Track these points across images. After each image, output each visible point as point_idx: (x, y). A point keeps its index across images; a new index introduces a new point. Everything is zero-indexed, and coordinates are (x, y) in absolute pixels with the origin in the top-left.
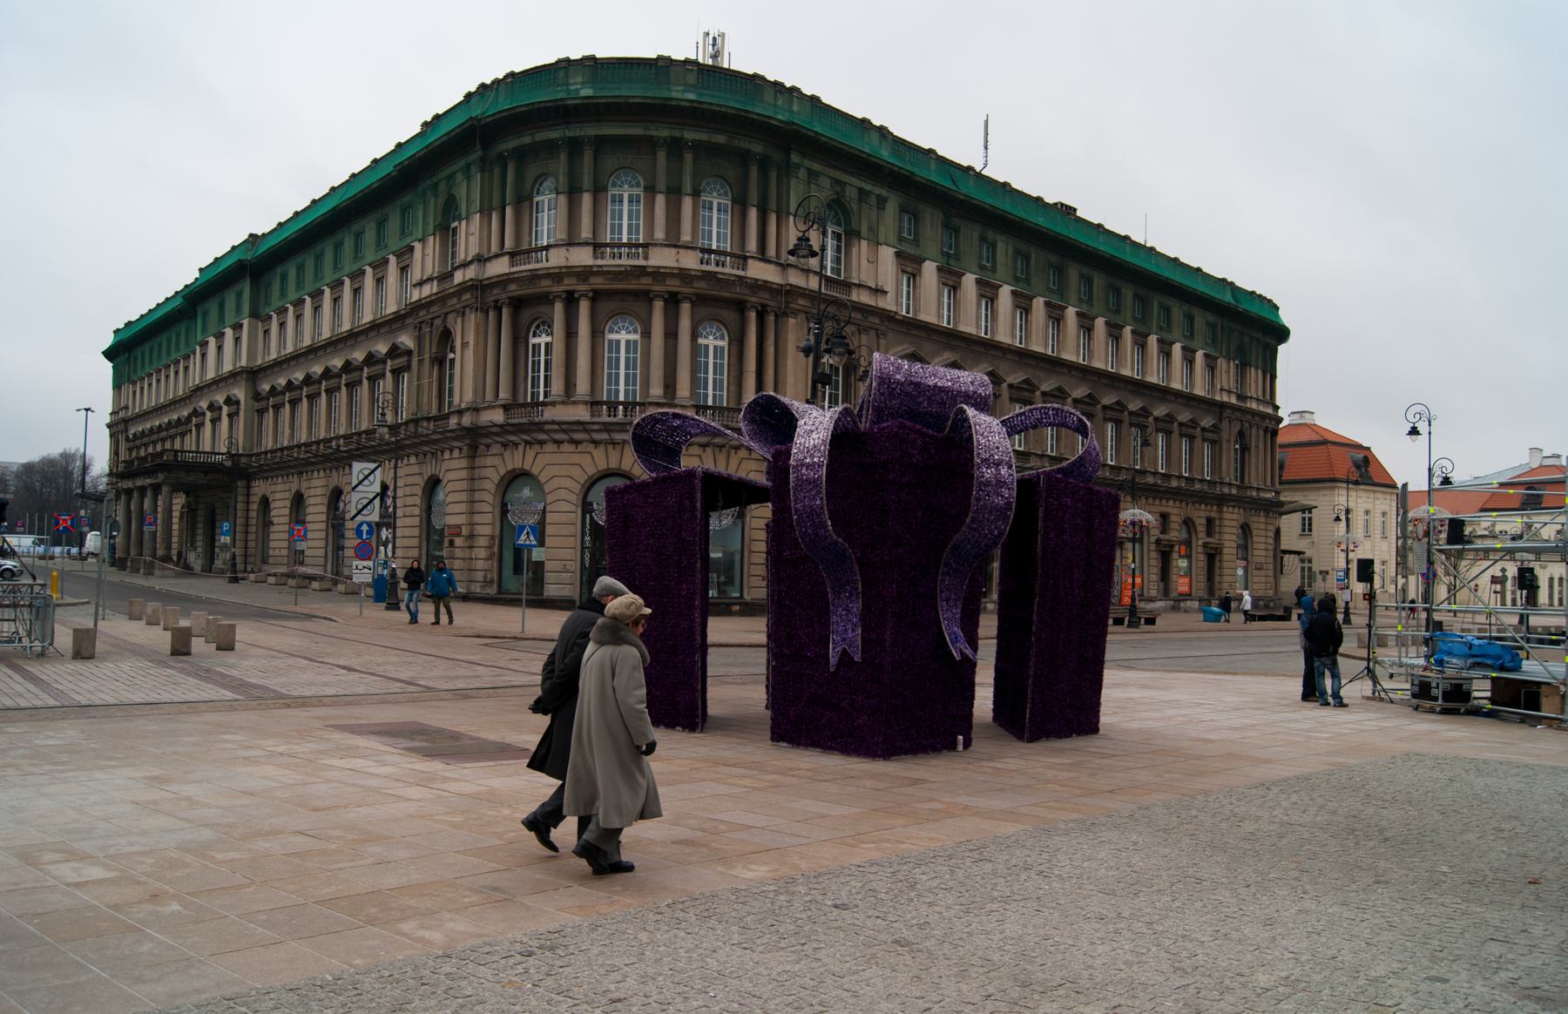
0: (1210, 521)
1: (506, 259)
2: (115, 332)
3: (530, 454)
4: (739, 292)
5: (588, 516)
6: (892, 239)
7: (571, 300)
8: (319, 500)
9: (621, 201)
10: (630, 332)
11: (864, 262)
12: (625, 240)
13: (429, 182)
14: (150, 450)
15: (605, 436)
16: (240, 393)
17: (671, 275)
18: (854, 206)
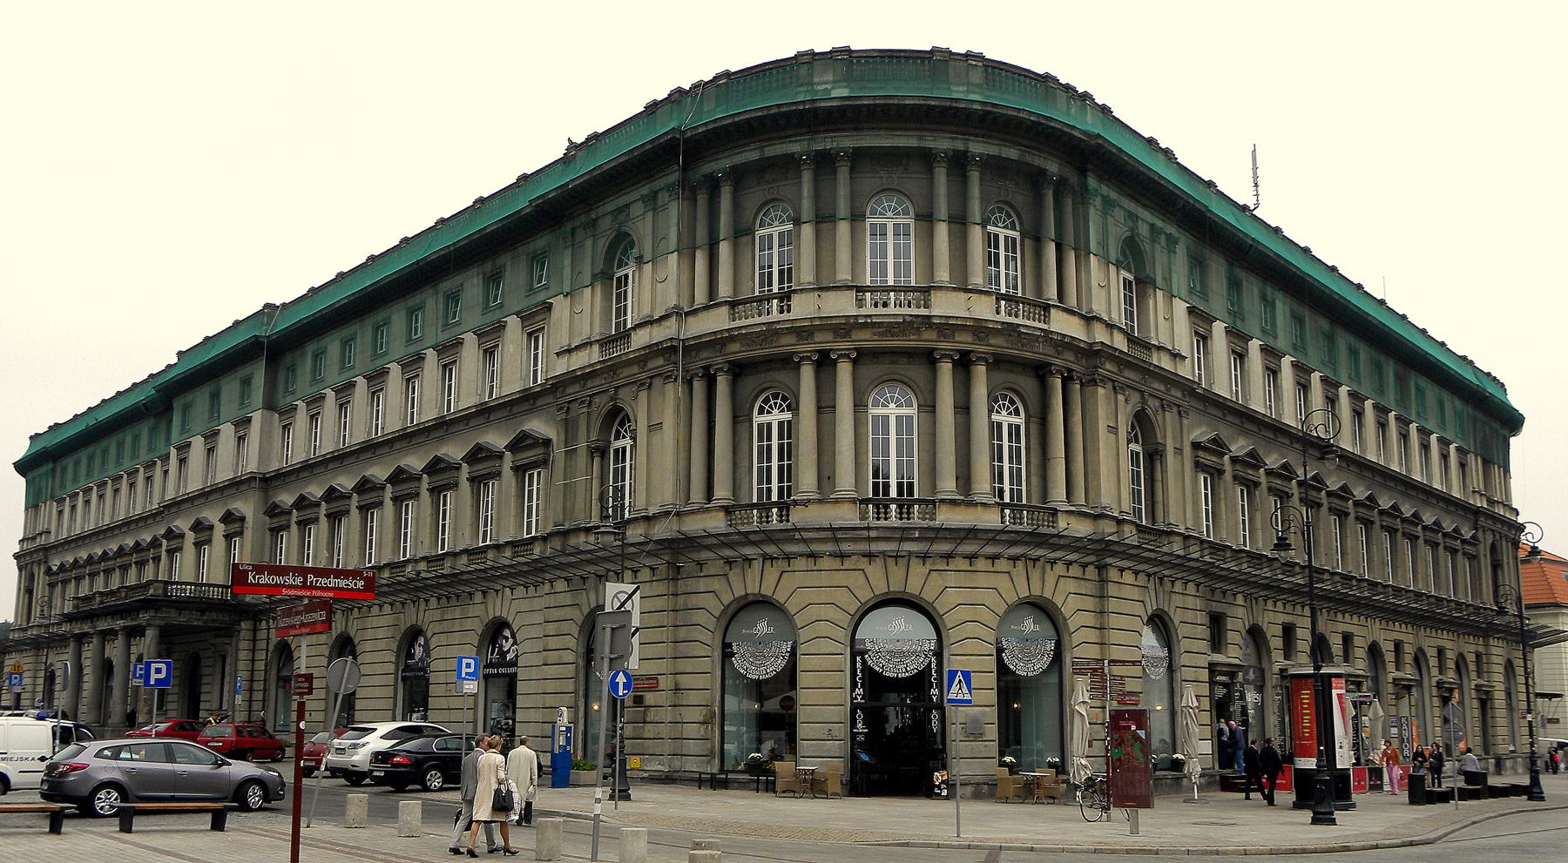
0: (1478, 656)
1: (724, 310)
2: (31, 438)
3: (772, 573)
4: (1040, 352)
5: (858, 659)
6: (1184, 294)
7: (825, 363)
8: (381, 645)
10: (1010, 414)
11: (1161, 319)
12: (891, 282)
13: (583, 218)
14: (99, 585)
15: (829, 547)
16: (247, 507)
17: (963, 328)
18: (1148, 247)
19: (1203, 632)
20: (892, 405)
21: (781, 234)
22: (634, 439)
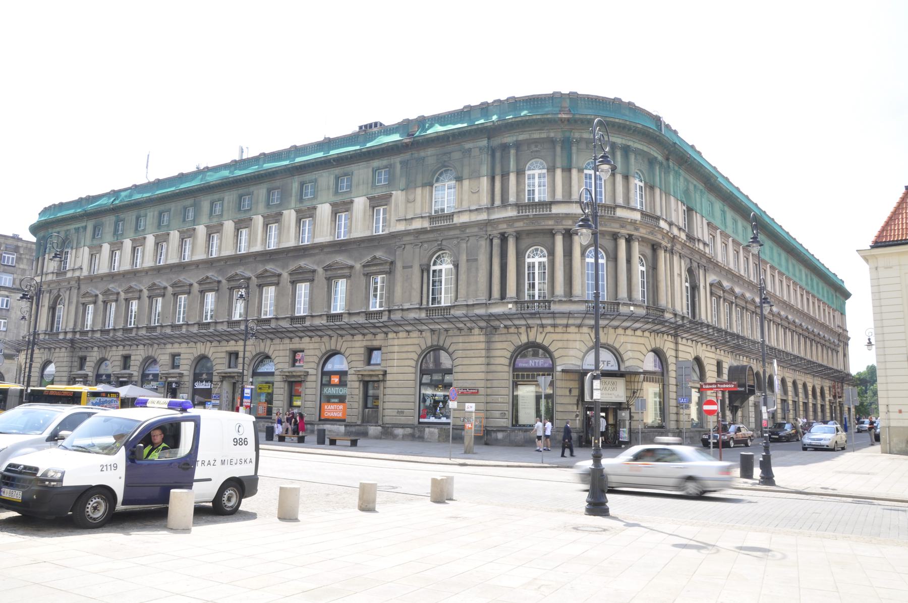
9: (534, 178)
10: (541, 257)
19: (715, 368)
21: (539, 174)
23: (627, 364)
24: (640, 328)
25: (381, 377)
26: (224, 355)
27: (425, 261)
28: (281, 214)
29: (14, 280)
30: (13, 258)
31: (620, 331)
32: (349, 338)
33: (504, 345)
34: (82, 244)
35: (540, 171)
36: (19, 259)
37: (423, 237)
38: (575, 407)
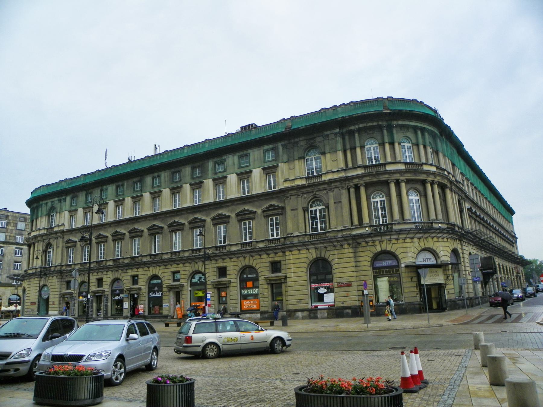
9: (371, 150)
10: (381, 197)
20: (413, 196)
22: (53, 249)
23: (442, 259)
24: (435, 236)
25: (283, 280)
26: (170, 274)
27: (306, 205)
28: (202, 182)
29: (6, 236)
30: (5, 223)
31: (435, 239)
32: (258, 257)
33: (366, 253)
34: (64, 210)
35: (374, 146)
36: (8, 223)
37: (303, 190)
38: (416, 288)
